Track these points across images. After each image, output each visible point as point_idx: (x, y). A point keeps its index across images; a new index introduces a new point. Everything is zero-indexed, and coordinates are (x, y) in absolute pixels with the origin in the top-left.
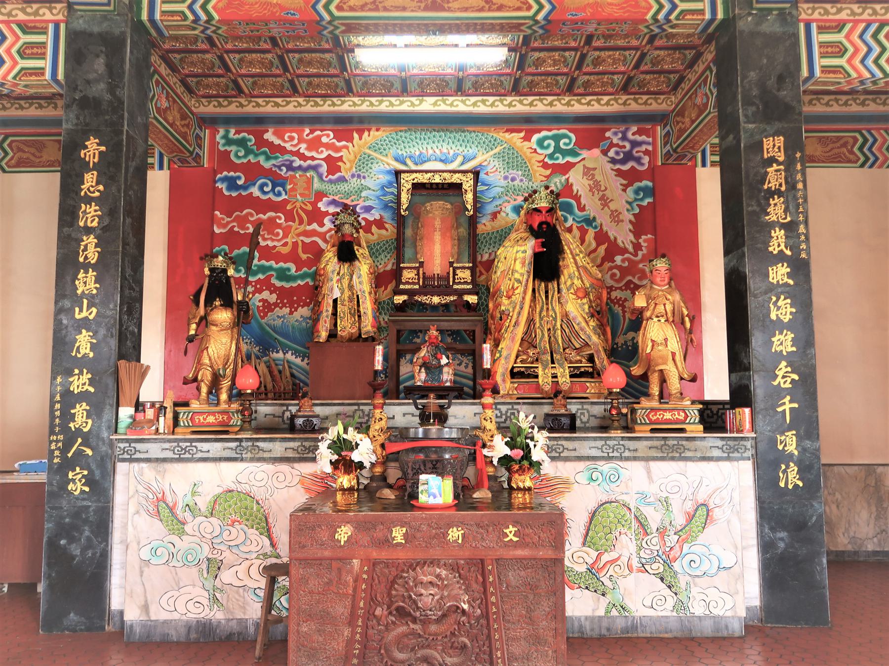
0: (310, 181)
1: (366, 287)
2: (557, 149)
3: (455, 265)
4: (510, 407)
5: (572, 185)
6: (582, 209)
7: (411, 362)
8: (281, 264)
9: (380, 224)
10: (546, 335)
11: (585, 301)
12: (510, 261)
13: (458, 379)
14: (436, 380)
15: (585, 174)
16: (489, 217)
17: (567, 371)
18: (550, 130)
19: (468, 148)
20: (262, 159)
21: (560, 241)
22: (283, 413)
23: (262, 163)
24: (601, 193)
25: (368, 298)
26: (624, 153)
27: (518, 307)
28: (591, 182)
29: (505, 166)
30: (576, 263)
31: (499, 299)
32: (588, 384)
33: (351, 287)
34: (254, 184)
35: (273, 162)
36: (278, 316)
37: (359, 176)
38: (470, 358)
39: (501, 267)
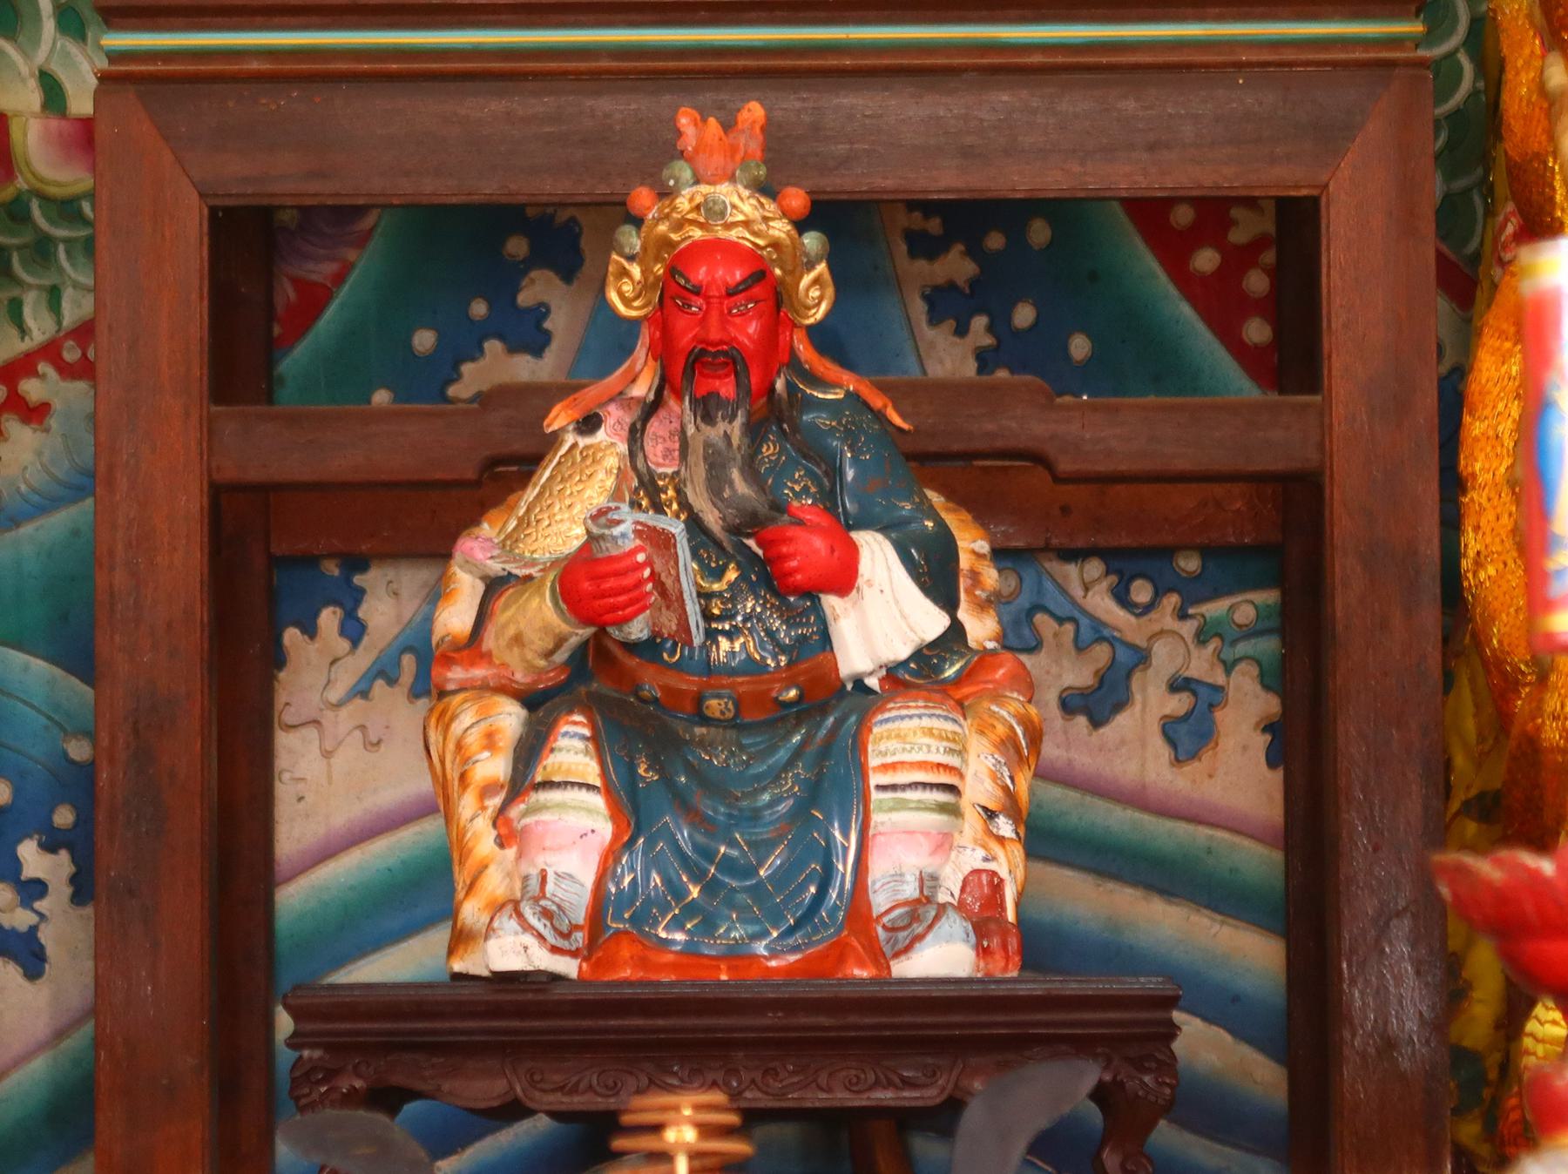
7: (425, 669)
13: (1084, 900)
14: (764, 904)
38: (1245, 607)
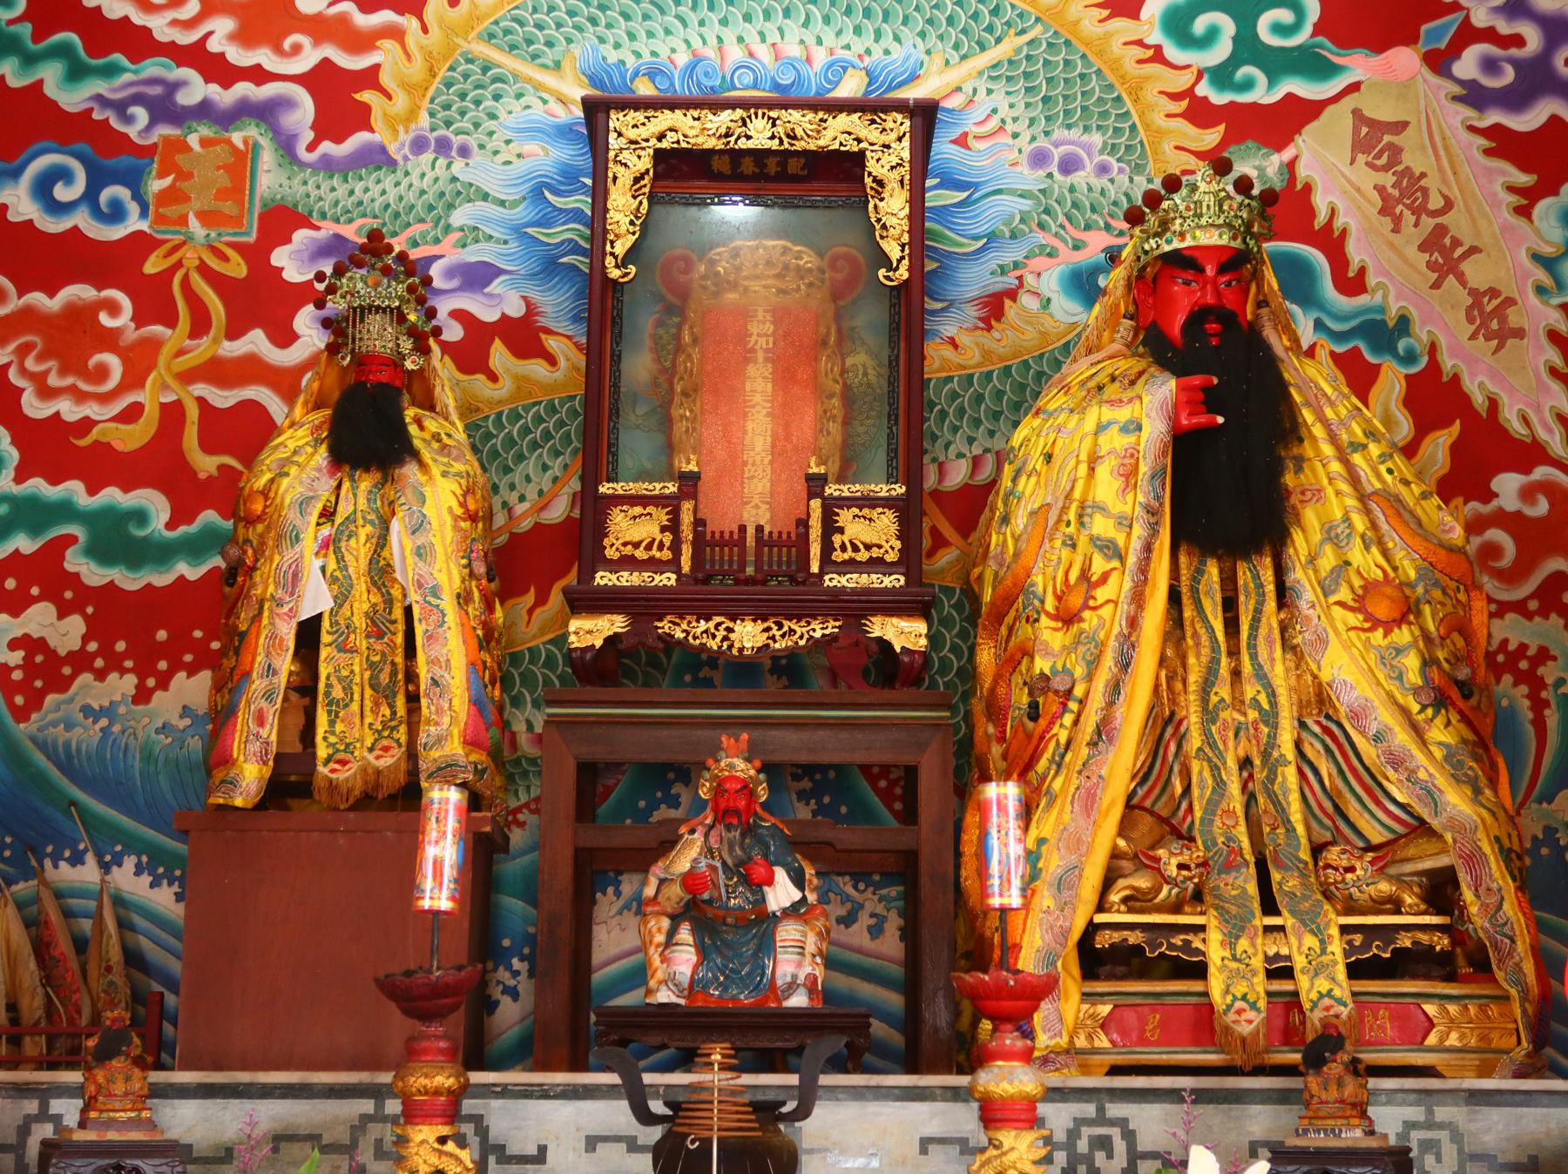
0: (241, 165)
1: (447, 574)
2: (1248, 48)
3: (831, 490)
4: (1089, 1109)
5: (1308, 188)
6: (1352, 284)
8: (112, 495)
9: (523, 335)
10: (1234, 788)
11: (1403, 635)
12: (1071, 467)
13: (843, 982)
14: (744, 983)
15: (1359, 146)
16: (972, 312)
17: (1336, 947)
19: (888, 41)
20: (51, 75)
21: (1282, 388)
22: (24, 1131)
23: (50, 90)
24: (1428, 223)
25: (452, 617)
26: (1514, 62)
27: (1109, 661)
28: (1388, 179)
29: (1037, 112)
30: (1354, 479)
31: (1024, 630)
32: (1430, 1009)
33: (381, 573)
34: (16, 174)
35: (99, 86)
36: (87, 710)
37: (443, 146)
38: (894, 891)
39: (1028, 495)
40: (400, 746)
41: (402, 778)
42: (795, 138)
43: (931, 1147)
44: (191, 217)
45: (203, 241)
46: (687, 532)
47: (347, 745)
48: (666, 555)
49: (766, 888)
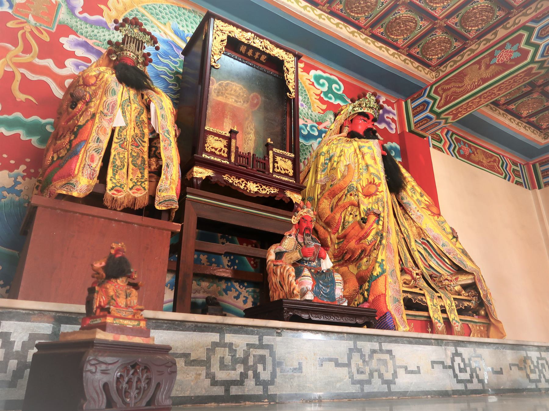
18: (324, 72)
40: (145, 189)
41: (146, 202)
42: (267, 49)
43: (416, 369)
44: (30, 16)
45: (33, 24)
46: (233, 149)
47: (121, 185)
48: (225, 155)
49: (322, 260)
